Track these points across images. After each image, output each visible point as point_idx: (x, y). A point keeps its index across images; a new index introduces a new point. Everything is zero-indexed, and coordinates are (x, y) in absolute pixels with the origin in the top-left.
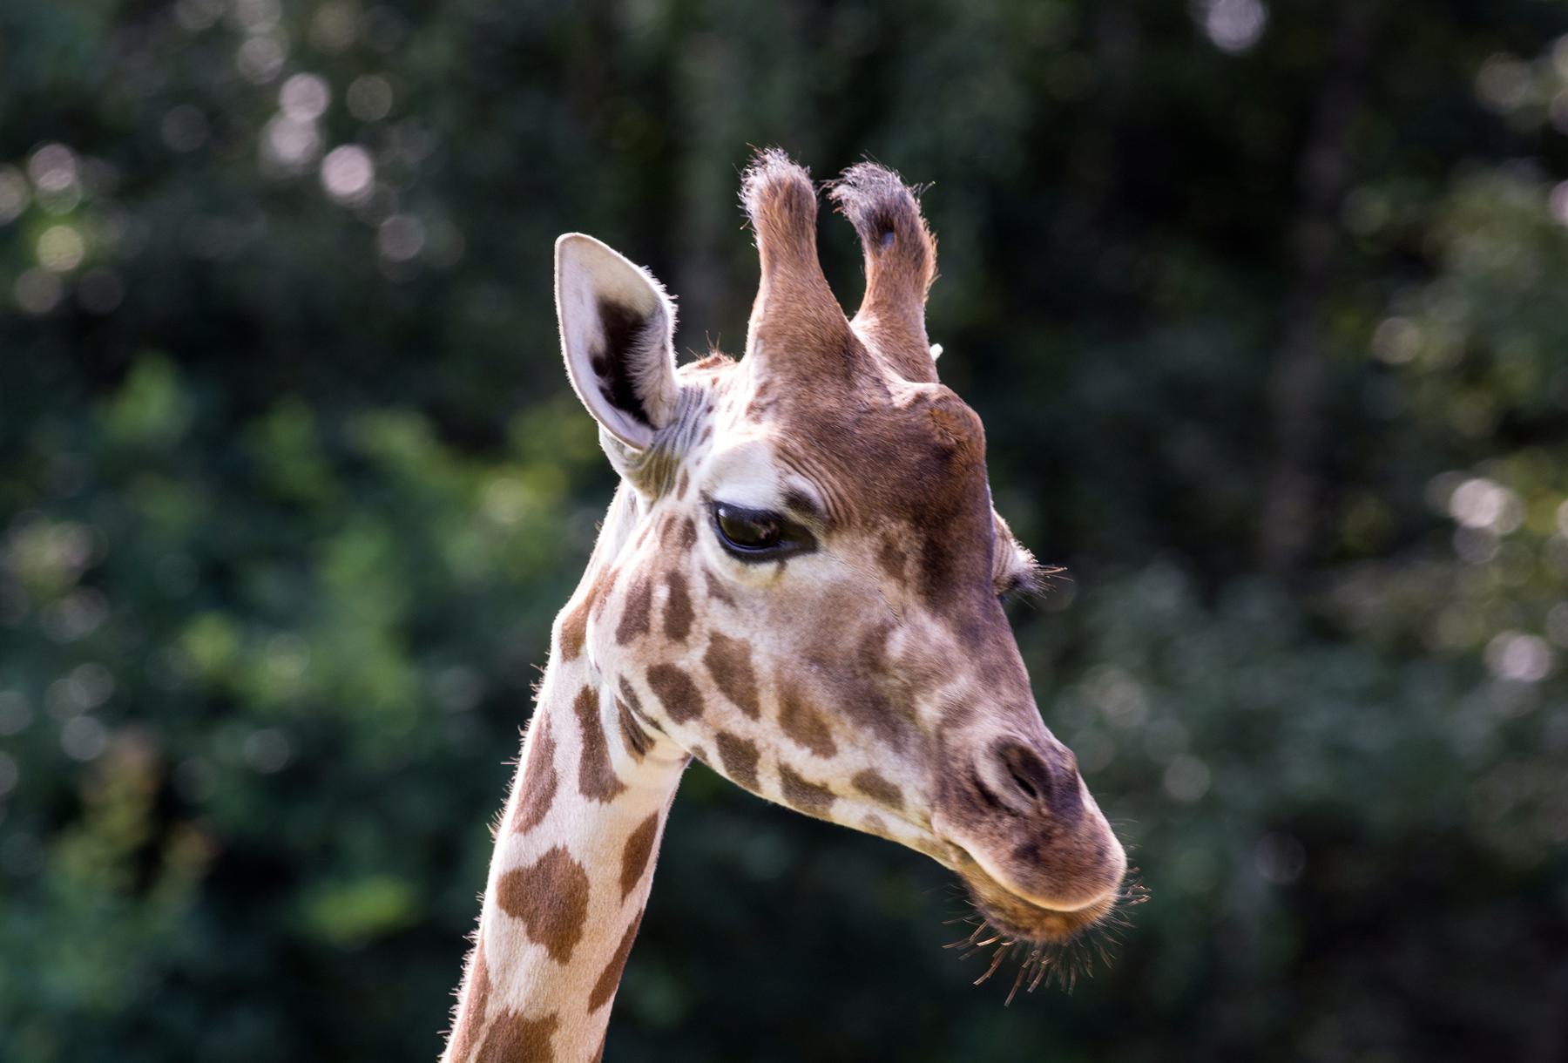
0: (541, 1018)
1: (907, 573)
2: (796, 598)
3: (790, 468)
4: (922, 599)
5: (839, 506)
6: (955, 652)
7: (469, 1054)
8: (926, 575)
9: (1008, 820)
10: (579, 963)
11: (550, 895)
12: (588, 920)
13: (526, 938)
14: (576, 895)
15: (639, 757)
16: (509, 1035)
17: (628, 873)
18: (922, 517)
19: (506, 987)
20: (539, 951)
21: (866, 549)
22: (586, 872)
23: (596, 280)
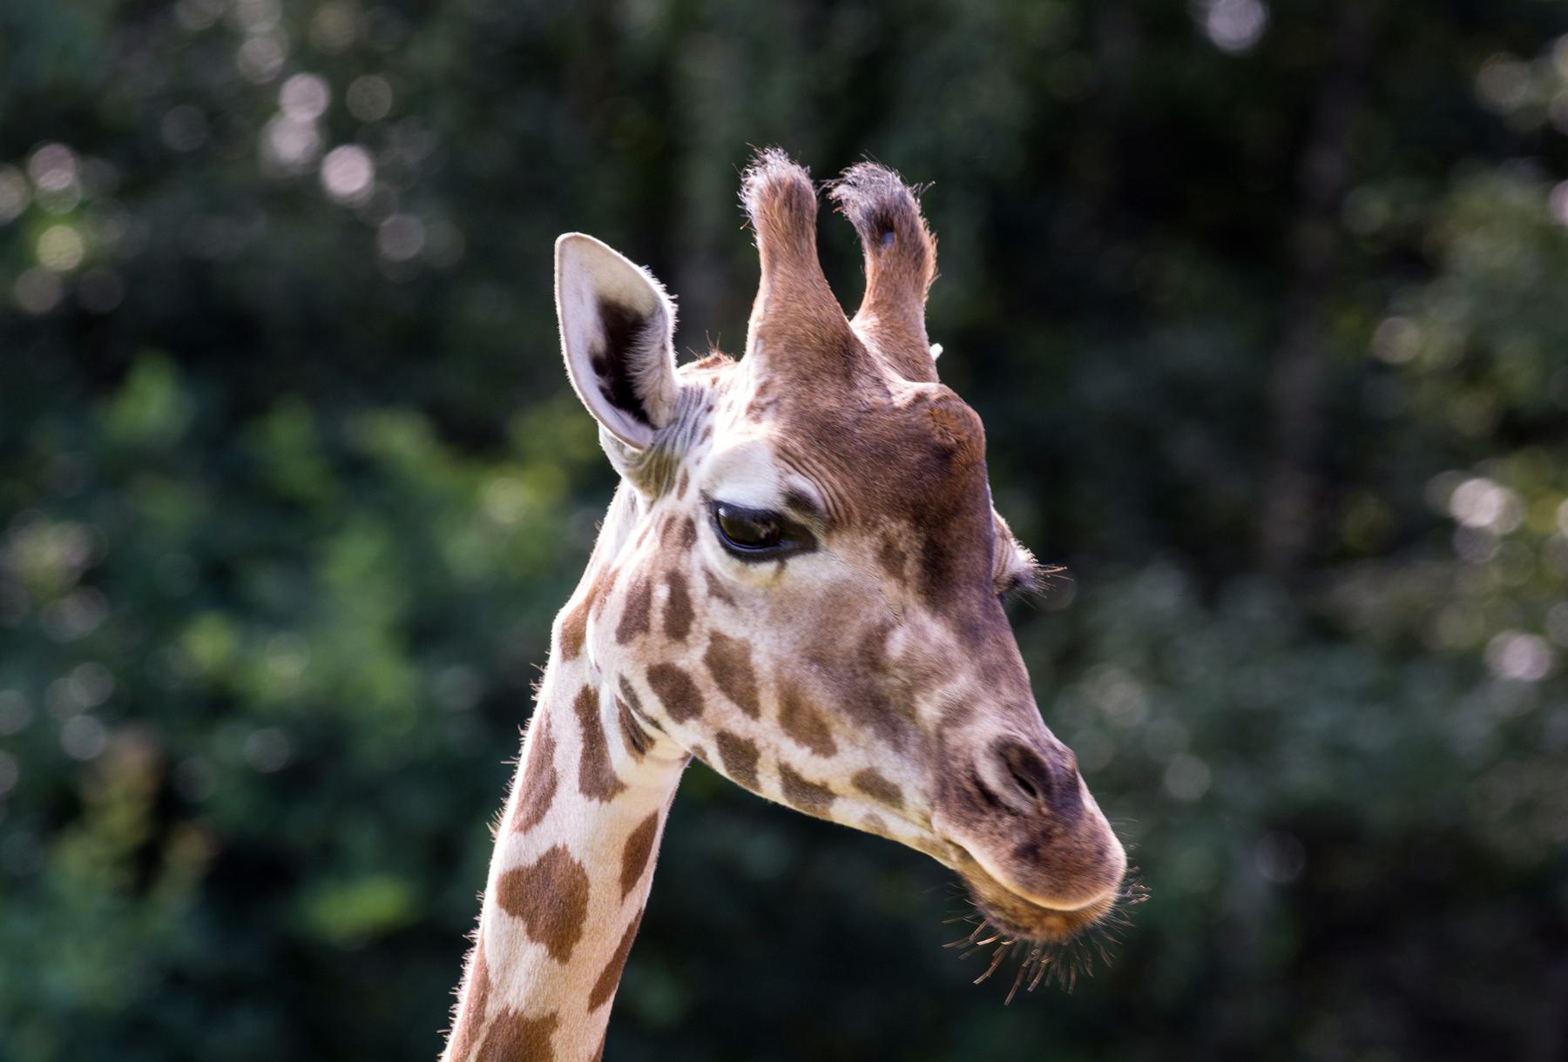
0: (541, 1017)
1: (907, 573)
2: (796, 598)
3: (790, 468)
4: (922, 598)
5: (839, 505)
6: (955, 651)
7: (469, 1053)
8: (926, 574)
9: (1008, 820)
10: (579, 962)
11: (550, 894)
12: (588, 919)
13: (526, 937)
14: (576, 894)
15: (639, 756)
16: (509, 1034)
17: (628, 872)
18: (922, 516)
19: (506, 986)
20: (539, 950)
21: (866, 548)
22: (586, 872)
23: (596, 279)
